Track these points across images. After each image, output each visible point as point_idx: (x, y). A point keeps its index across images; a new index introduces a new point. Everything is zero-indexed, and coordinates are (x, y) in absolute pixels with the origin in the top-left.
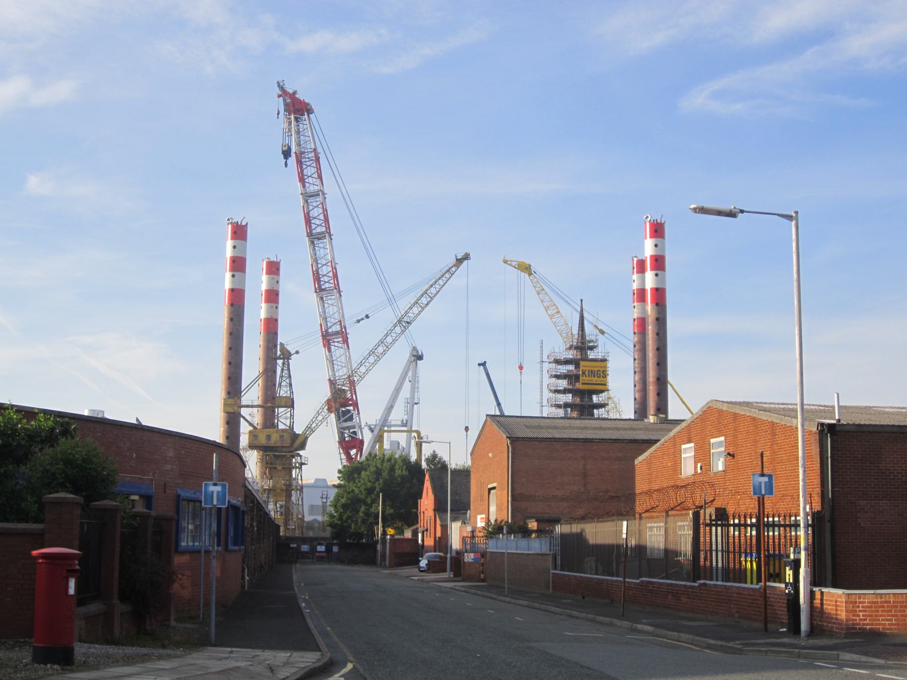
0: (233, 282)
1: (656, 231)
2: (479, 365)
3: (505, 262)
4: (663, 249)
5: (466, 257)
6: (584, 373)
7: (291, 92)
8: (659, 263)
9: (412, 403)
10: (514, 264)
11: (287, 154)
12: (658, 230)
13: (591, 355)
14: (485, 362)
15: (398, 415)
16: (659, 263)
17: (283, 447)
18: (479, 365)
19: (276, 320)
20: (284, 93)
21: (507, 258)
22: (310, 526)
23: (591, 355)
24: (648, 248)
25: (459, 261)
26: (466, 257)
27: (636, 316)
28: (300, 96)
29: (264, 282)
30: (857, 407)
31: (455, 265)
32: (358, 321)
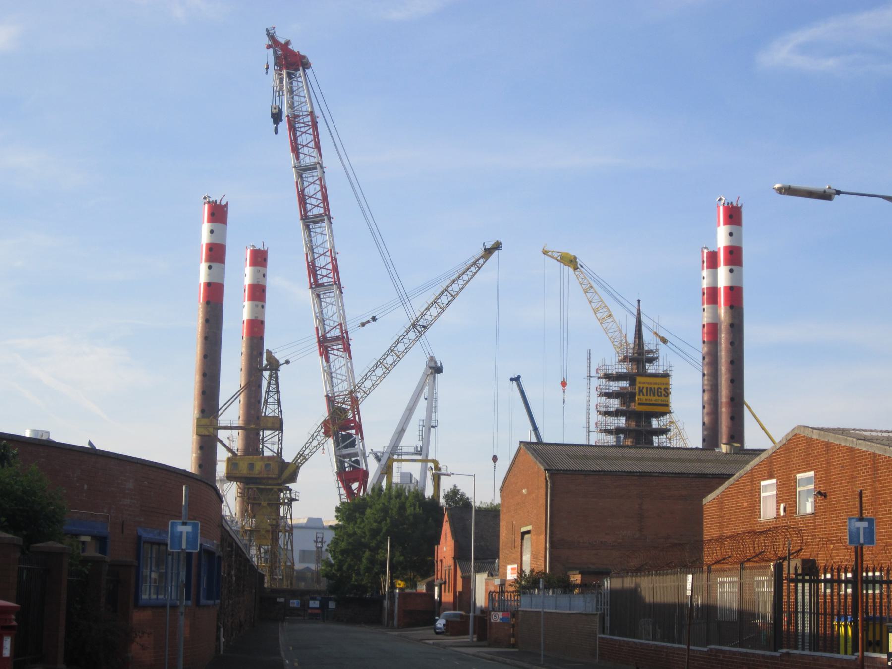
0: (209, 275)
2: (512, 379)
3: (545, 253)
4: (740, 239)
5: (497, 246)
7: (283, 42)
9: (429, 426)
10: (556, 255)
11: (277, 118)
12: (733, 216)
13: (651, 369)
15: (411, 441)
16: (734, 256)
20: (274, 43)
21: (547, 249)
23: (651, 369)
24: (722, 238)
25: (488, 252)
26: (497, 246)
27: (705, 321)
28: (295, 47)
29: (248, 276)
31: (482, 257)
32: (363, 324)
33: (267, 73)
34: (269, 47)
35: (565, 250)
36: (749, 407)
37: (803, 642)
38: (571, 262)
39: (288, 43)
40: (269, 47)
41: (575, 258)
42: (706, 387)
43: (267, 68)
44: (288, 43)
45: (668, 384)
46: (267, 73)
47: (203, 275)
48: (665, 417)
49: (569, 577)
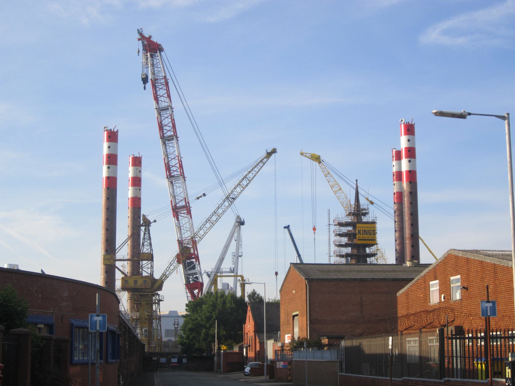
0: (108, 172)
2: (285, 228)
3: (302, 154)
4: (414, 142)
5: (274, 151)
7: (147, 36)
10: (308, 155)
11: (145, 80)
12: (410, 130)
13: (365, 219)
15: (227, 265)
16: (411, 153)
18: (285, 228)
19: (140, 199)
20: (142, 38)
21: (303, 152)
23: (365, 219)
24: (403, 143)
25: (269, 154)
26: (274, 151)
27: (395, 191)
28: (154, 39)
29: (131, 172)
31: (266, 157)
32: (198, 198)
33: (138, 55)
35: (313, 152)
36: (421, 240)
37: (457, 374)
38: (317, 159)
39: (150, 37)
40: (139, 40)
41: (319, 157)
42: (397, 229)
43: (139, 52)
44: (150, 37)
45: (375, 227)
46: (138, 55)
47: (105, 172)
48: (374, 247)
49: (321, 341)
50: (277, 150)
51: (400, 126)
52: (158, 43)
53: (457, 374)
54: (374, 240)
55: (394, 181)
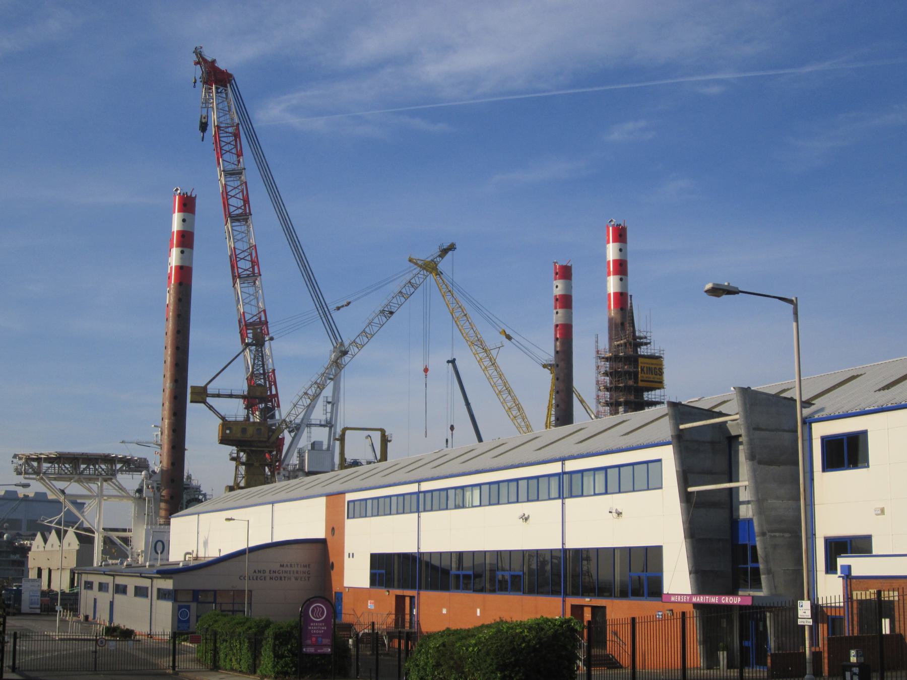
0: (182, 259)
1: (620, 236)
2: (448, 362)
3: (410, 261)
4: (626, 254)
5: (452, 248)
6: (642, 370)
7: (210, 59)
8: (621, 267)
9: (334, 403)
10: (420, 263)
11: (204, 127)
12: (621, 235)
13: (643, 351)
14: (454, 360)
15: (319, 414)
17: (260, 442)
18: (448, 362)
20: (201, 60)
21: (413, 257)
22: (738, 509)
23: (643, 351)
24: (612, 252)
26: (452, 248)
27: (554, 322)
28: (221, 65)
30: (73, 454)
31: (440, 256)
33: (194, 86)
34: (197, 63)
36: (579, 396)
37: (565, 588)
39: (214, 61)
40: (197, 63)
43: (195, 82)
44: (214, 61)
45: (661, 365)
46: (194, 86)
47: (174, 258)
48: (653, 392)
50: (457, 246)
51: (606, 229)
52: (229, 71)
53: (565, 588)
54: (661, 382)
55: (556, 308)
